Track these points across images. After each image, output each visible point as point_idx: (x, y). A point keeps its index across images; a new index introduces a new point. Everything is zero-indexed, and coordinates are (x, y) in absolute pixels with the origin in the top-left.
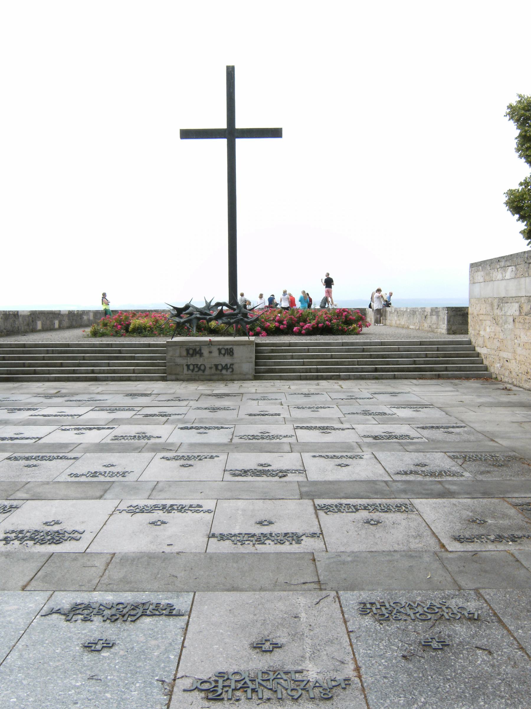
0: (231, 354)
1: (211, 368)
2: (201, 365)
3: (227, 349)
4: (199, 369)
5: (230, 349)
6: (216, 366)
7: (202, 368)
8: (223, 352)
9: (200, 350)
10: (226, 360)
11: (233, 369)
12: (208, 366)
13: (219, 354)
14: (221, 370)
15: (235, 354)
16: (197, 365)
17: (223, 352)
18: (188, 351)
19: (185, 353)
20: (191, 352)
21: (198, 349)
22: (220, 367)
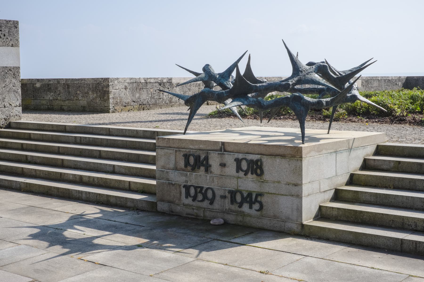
0: (259, 171)
1: (223, 197)
2: (207, 189)
3: (252, 161)
4: (205, 197)
5: (257, 161)
6: (233, 193)
7: (210, 194)
8: (244, 165)
9: (207, 158)
10: (249, 184)
11: (261, 203)
12: (219, 193)
13: (237, 172)
14: (241, 206)
15: (266, 173)
16: (202, 188)
17: (244, 165)
18: (186, 157)
19: (182, 164)
20: (192, 160)
21: (202, 157)
22: (239, 198)
